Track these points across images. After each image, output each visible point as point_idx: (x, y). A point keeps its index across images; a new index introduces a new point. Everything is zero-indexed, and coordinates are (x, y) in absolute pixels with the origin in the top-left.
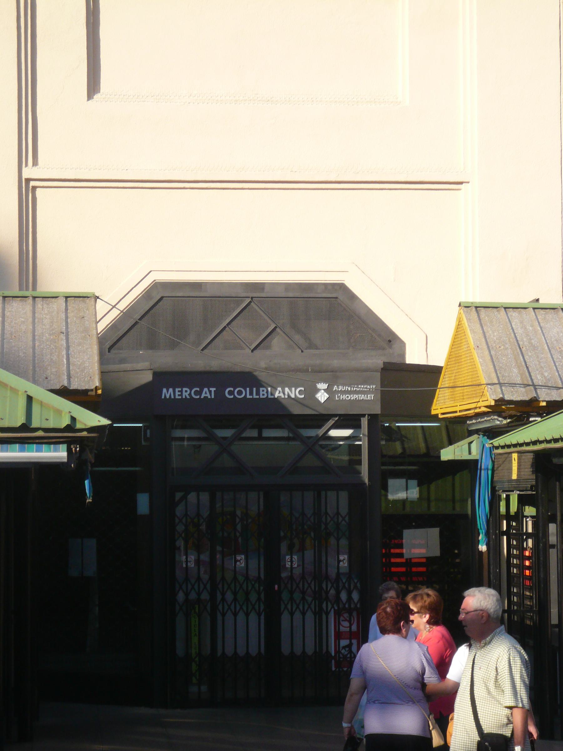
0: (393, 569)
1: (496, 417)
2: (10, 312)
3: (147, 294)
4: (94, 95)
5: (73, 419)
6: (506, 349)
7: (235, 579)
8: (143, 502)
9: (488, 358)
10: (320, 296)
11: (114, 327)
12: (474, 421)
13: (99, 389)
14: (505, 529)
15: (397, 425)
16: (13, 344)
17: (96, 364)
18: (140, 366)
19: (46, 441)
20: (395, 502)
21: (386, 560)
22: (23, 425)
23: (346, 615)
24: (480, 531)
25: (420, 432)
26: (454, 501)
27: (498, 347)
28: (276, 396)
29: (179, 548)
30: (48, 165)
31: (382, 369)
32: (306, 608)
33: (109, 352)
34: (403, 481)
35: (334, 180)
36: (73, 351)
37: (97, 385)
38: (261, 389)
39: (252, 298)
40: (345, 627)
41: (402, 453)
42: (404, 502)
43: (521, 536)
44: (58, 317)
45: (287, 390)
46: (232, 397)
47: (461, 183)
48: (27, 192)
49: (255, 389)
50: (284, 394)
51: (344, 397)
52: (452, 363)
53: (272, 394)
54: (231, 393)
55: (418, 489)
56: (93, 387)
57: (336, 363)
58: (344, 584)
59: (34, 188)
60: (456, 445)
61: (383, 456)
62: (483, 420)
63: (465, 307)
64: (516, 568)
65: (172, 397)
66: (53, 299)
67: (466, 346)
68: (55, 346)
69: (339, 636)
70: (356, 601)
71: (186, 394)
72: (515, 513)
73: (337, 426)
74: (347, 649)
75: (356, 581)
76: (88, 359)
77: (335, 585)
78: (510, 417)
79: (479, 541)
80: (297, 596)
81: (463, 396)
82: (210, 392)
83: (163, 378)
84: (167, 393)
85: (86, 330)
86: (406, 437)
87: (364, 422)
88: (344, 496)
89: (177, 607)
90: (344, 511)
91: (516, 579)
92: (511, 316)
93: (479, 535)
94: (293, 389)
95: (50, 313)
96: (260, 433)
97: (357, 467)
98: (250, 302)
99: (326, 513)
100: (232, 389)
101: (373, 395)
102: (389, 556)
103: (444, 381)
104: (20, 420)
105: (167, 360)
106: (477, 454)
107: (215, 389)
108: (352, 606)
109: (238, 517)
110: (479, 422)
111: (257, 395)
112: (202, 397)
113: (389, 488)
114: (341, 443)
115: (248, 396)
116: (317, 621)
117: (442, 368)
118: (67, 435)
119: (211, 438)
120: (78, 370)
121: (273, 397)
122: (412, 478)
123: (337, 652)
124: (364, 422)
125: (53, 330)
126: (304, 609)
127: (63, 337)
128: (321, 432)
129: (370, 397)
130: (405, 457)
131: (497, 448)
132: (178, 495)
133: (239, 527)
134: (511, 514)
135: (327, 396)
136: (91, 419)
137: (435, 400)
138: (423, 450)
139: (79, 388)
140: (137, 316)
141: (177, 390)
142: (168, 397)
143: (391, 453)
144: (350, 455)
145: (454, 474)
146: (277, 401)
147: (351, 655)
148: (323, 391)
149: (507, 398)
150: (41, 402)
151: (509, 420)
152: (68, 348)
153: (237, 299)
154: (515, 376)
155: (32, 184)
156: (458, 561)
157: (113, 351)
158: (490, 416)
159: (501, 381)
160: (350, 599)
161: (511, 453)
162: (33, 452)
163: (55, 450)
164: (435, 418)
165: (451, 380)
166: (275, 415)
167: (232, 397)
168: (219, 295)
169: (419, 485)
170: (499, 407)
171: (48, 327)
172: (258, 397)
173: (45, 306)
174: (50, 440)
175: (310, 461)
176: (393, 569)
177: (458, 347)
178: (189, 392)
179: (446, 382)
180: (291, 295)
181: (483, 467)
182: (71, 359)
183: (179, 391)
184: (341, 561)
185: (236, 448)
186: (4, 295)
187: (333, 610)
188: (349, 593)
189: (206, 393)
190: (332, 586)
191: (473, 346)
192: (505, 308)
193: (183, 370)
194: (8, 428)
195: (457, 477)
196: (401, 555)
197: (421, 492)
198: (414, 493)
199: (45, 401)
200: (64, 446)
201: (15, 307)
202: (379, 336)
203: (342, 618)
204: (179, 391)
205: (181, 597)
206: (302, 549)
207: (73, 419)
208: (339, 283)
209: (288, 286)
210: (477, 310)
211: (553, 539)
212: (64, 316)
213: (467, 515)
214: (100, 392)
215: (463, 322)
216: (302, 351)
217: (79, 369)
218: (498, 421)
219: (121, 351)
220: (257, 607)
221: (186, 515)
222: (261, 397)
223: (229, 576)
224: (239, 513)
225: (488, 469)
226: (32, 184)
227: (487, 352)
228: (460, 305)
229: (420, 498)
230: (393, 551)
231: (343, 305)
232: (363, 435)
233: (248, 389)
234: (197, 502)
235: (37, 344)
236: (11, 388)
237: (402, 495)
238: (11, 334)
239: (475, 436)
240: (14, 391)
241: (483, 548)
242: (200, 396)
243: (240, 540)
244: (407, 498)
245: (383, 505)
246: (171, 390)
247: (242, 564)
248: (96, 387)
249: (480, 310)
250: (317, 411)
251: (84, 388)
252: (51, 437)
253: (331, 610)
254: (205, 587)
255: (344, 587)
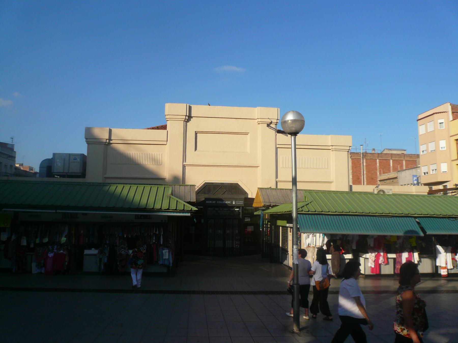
11: (198, 190)
30: (187, 163)
42: (247, 221)
43: (268, 228)
48: (184, 167)
57: (236, 197)
69: (236, 244)
83: (206, 199)
84: (207, 202)
95: (187, 188)
103: (255, 201)
104: (183, 209)
105: (207, 196)
118: (190, 211)
136: (194, 209)
153: (219, 186)
154: (267, 201)
166: (226, 206)
170: (264, 206)
198: (249, 220)
211: (273, 228)
237: (247, 220)
252: (188, 212)
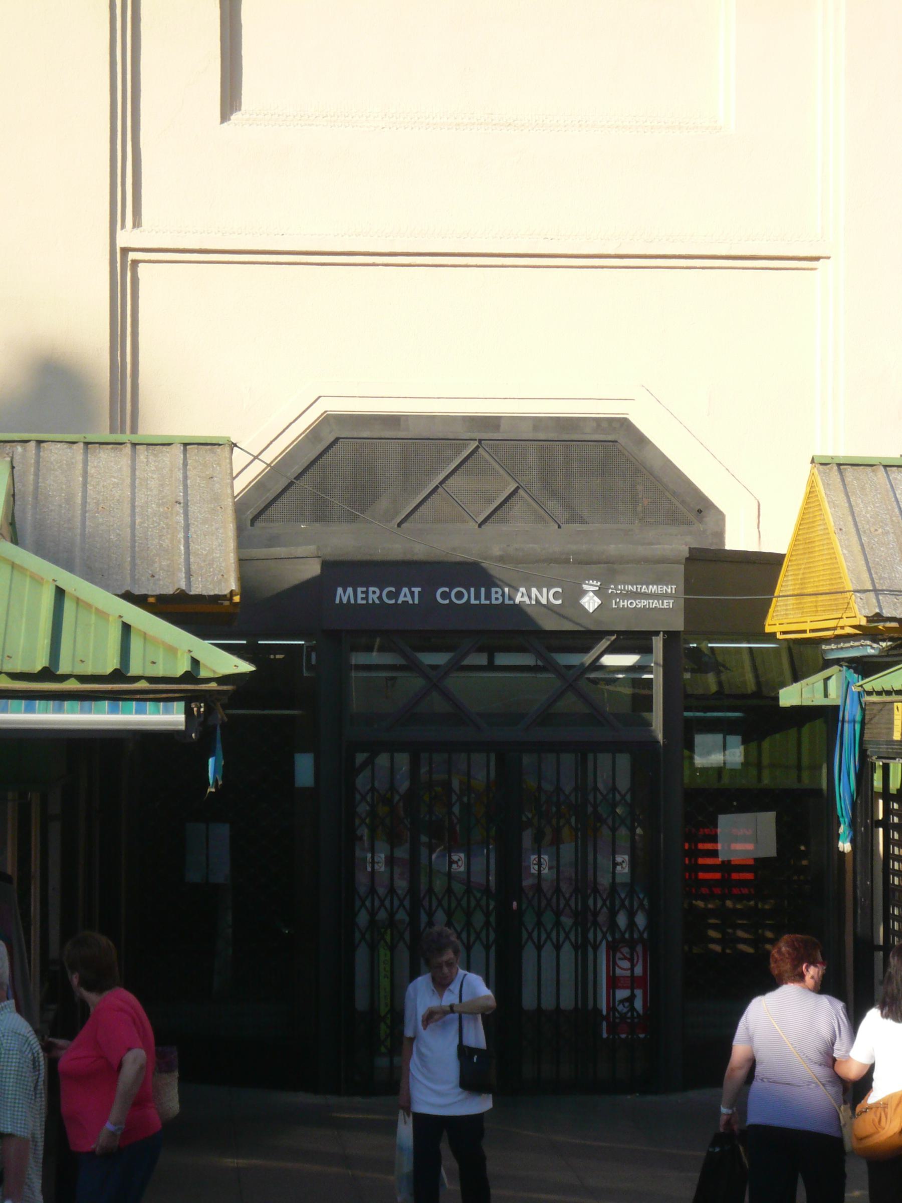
0: (702, 875)
1: (869, 643)
2: (95, 467)
3: (314, 433)
4: (232, 114)
5: (195, 662)
6: (888, 533)
7: (449, 891)
8: (304, 769)
9: (857, 548)
10: (588, 437)
11: (260, 485)
12: (833, 646)
13: (236, 595)
14: (881, 817)
15: (710, 645)
16: (101, 520)
17: (232, 554)
18: (300, 551)
19: (151, 696)
20: (705, 770)
21: (690, 861)
22: (116, 671)
23: (626, 950)
24: (841, 820)
25: (746, 658)
26: (799, 768)
27: (872, 529)
28: (517, 601)
29: (361, 838)
31: (687, 559)
32: (561, 940)
33: (252, 524)
34: (719, 737)
35: (612, 252)
36: (195, 532)
37: (234, 588)
38: (493, 590)
39: (480, 441)
40: (625, 969)
41: (717, 693)
42: (719, 771)
44: (171, 477)
45: (534, 591)
46: (447, 602)
47: (817, 259)
48: (124, 269)
49: (483, 590)
50: (530, 598)
51: (625, 603)
52: (799, 552)
53: (510, 598)
54: (445, 595)
55: (742, 748)
56: (226, 592)
57: (613, 549)
58: (623, 901)
59: (135, 263)
60: (804, 682)
61: (687, 696)
62: (847, 645)
63: (822, 464)
64: (898, 877)
65: (352, 601)
66: (164, 448)
67: (822, 527)
68: (167, 524)
69: (613, 983)
70: (641, 928)
71: (373, 598)
72: (898, 790)
73: (613, 649)
74: (627, 1004)
75: (641, 896)
76: (219, 545)
77: (608, 903)
78: (891, 639)
79: (839, 835)
80: (548, 918)
81: (816, 606)
82: (412, 593)
83: (338, 571)
84: (344, 595)
85: (216, 498)
86: (724, 666)
87: (658, 643)
88: (624, 761)
89: (357, 936)
90: (624, 783)
91: (897, 894)
92: (896, 479)
93: (839, 825)
94: (545, 590)
95: (160, 470)
96: (491, 659)
97: (645, 715)
98: (478, 447)
99: (596, 789)
100: (447, 590)
101: (671, 601)
102: (694, 853)
103: (786, 583)
104: (111, 664)
105: (346, 540)
106: (838, 696)
107: (420, 589)
108: (636, 936)
109: (456, 794)
110: (842, 648)
111: (486, 599)
112: (400, 602)
113: (696, 749)
114: (620, 676)
115: (473, 601)
116: (579, 962)
117: (783, 556)
118: (186, 687)
119: (412, 666)
120: (203, 564)
121: (512, 602)
122: (732, 733)
123: (611, 1008)
124: (658, 643)
125: (163, 497)
126: (558, 940)
127: (179, 509)
128: (588, 659)
129: (668, 604)
130: (723, 698)
131: (869, 693)
132: (360, 757)
133: (456, 809)
134: (891, 792)
135: (597, 601)
136: (222, 663)
137: (771, 610)
138: (751, 687)
139: (204, 593)
140: (297, 469)
141: (360, 590)
142: (345, 601)
143: (701, 691)
144: (634, 687)
145: (800, 725)
146: (518, 610)
147: (632, 1015)
148: (591, 594)
149: (886, 613)
150: (145, 634)
151: (889, 643)
152: (187, 527)
153: (456, 443)
155: (132, 256)
156: (805, 863)
157: (258, 524)
158: (859, 640)
159: (878, 587)
160: (632, 924)
161: (892, 702)
162: (131, 713)
163: (167, 712)
164: (772, 637)
165: (797, 579)
167: (447, 602)
168: (425, 435)
169: (744, 742)
171: (155, 492)
172: (488, 602)
173: (151, 458)
174: (158, 696)
175: (570, 703)
176: (702, 875)
177: (808, 528)
178: (378, 594)
179: (790, 583)
180: (542, 436)
181: (846, 718)
182: (192, 544)
183: (362, 592)
184: (617, 864)
185: (455, 682)
186: (86, 440)
187: (604, 942)
188: (631, 915)
189: (405, 596)
190: (604, 904)
191: (833, 529)
192: (885, 466)
193: (368, 558)
194: (92, 676)
195: (806, 729)
196: (714, 853)
197: (747, 754)
199: (151, 632)
200: (181, 705)
201: (103, 458)
202: (683, 502)
203: (618, 955)
204: (362, 592)
205: (363, 918)
206: (557, 841)
207: (195, 662)
208: (620, 418)
209: (538, 422)
210: (839, 469)
212: (181, 476)
213: (821, 790)
214: (237, 599)
215: (817, 489)
216: (559, 527)
217: (204, 561)
218: (870, 649)
219: (272, 525)
220: (483, 935)
221: (373, 789)
222: (494, 602)
223: (439, 885)
224: (456, 784)
225: (854, 722)
226: (132, 256)
227: (855, 539)
228: (813, 461)
229: (746, 764)
230: (701, 846)
231: (626, 453)
232: (656, 664)
233: (472, 590)
234: (392, 770)
235: (138, 520)
236: (97, 610)
237: (716, 759)
238: (97, 503)
239: (836, 668)
240: (102, 614)
241: (845, 846)
242: (396, 601)
243: (458, 828)
244: (725, 763)
245: (687, 772)
246: (350, 590)
247: (460, 868)
248: (232, 591)
249: (845, 469)
250: (582, 626)
251: (212, 593)
252: (160, 690)
253: (601, 942)
254: (402, 904)
255: (623, 905)
